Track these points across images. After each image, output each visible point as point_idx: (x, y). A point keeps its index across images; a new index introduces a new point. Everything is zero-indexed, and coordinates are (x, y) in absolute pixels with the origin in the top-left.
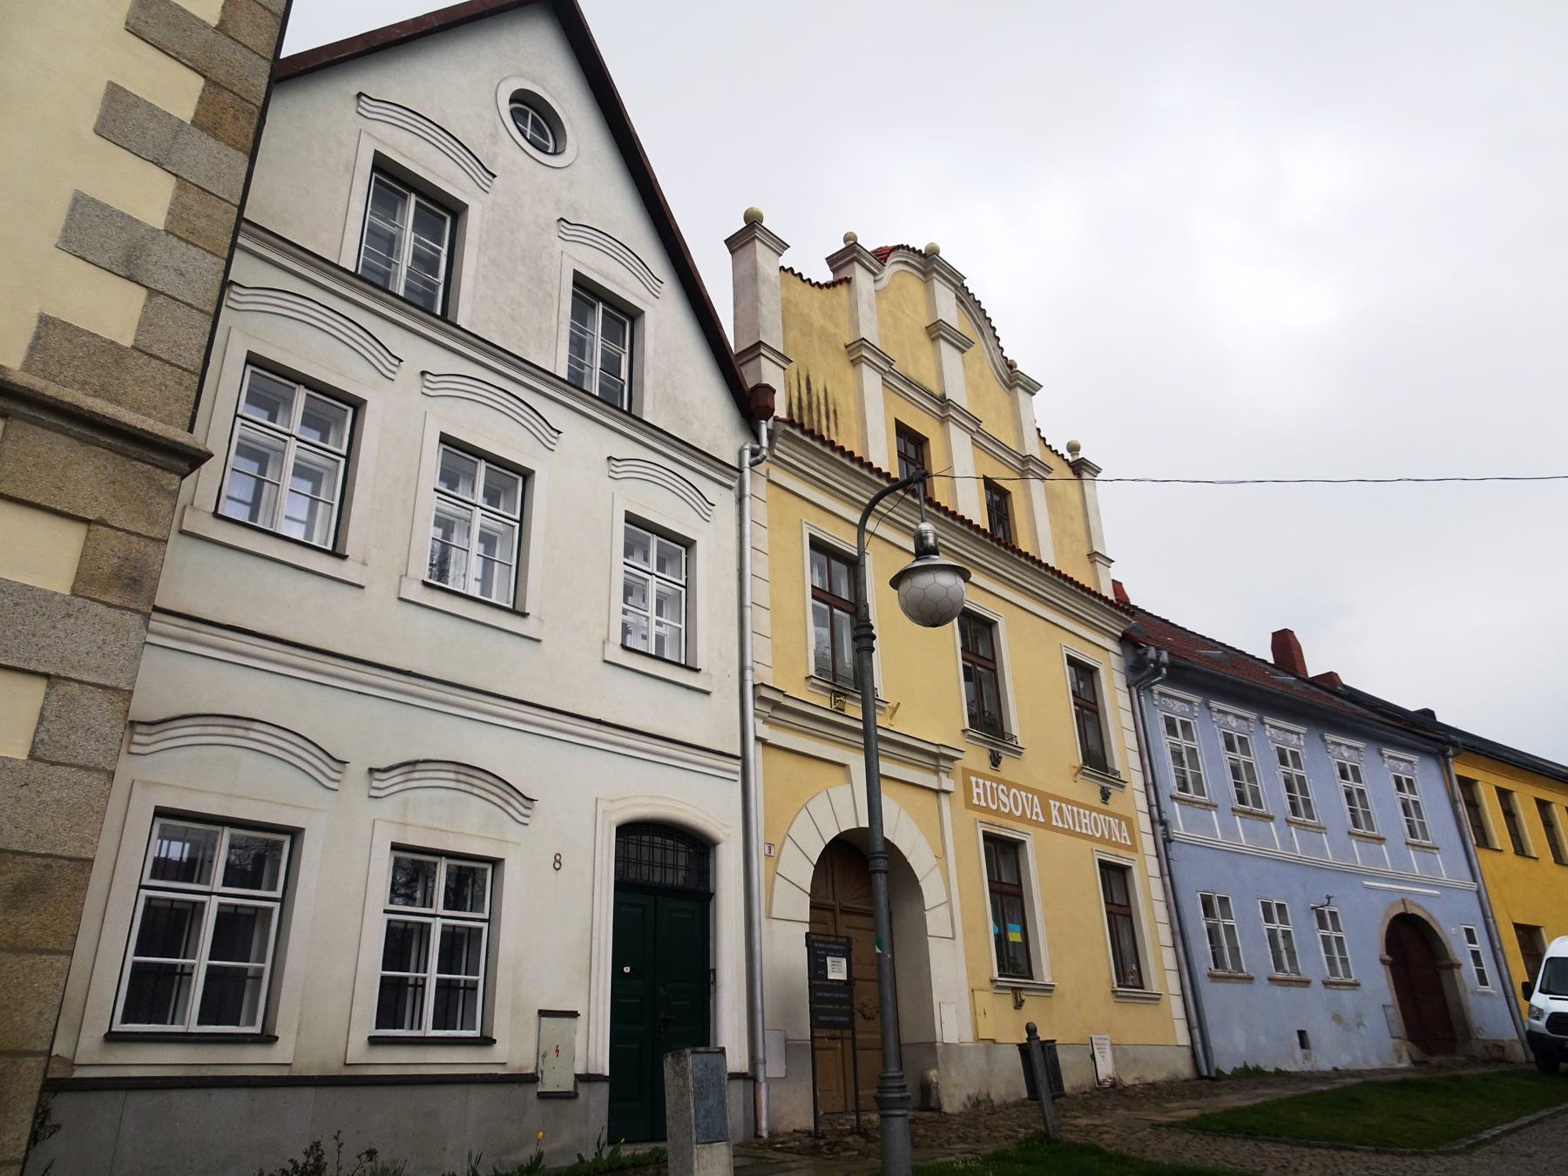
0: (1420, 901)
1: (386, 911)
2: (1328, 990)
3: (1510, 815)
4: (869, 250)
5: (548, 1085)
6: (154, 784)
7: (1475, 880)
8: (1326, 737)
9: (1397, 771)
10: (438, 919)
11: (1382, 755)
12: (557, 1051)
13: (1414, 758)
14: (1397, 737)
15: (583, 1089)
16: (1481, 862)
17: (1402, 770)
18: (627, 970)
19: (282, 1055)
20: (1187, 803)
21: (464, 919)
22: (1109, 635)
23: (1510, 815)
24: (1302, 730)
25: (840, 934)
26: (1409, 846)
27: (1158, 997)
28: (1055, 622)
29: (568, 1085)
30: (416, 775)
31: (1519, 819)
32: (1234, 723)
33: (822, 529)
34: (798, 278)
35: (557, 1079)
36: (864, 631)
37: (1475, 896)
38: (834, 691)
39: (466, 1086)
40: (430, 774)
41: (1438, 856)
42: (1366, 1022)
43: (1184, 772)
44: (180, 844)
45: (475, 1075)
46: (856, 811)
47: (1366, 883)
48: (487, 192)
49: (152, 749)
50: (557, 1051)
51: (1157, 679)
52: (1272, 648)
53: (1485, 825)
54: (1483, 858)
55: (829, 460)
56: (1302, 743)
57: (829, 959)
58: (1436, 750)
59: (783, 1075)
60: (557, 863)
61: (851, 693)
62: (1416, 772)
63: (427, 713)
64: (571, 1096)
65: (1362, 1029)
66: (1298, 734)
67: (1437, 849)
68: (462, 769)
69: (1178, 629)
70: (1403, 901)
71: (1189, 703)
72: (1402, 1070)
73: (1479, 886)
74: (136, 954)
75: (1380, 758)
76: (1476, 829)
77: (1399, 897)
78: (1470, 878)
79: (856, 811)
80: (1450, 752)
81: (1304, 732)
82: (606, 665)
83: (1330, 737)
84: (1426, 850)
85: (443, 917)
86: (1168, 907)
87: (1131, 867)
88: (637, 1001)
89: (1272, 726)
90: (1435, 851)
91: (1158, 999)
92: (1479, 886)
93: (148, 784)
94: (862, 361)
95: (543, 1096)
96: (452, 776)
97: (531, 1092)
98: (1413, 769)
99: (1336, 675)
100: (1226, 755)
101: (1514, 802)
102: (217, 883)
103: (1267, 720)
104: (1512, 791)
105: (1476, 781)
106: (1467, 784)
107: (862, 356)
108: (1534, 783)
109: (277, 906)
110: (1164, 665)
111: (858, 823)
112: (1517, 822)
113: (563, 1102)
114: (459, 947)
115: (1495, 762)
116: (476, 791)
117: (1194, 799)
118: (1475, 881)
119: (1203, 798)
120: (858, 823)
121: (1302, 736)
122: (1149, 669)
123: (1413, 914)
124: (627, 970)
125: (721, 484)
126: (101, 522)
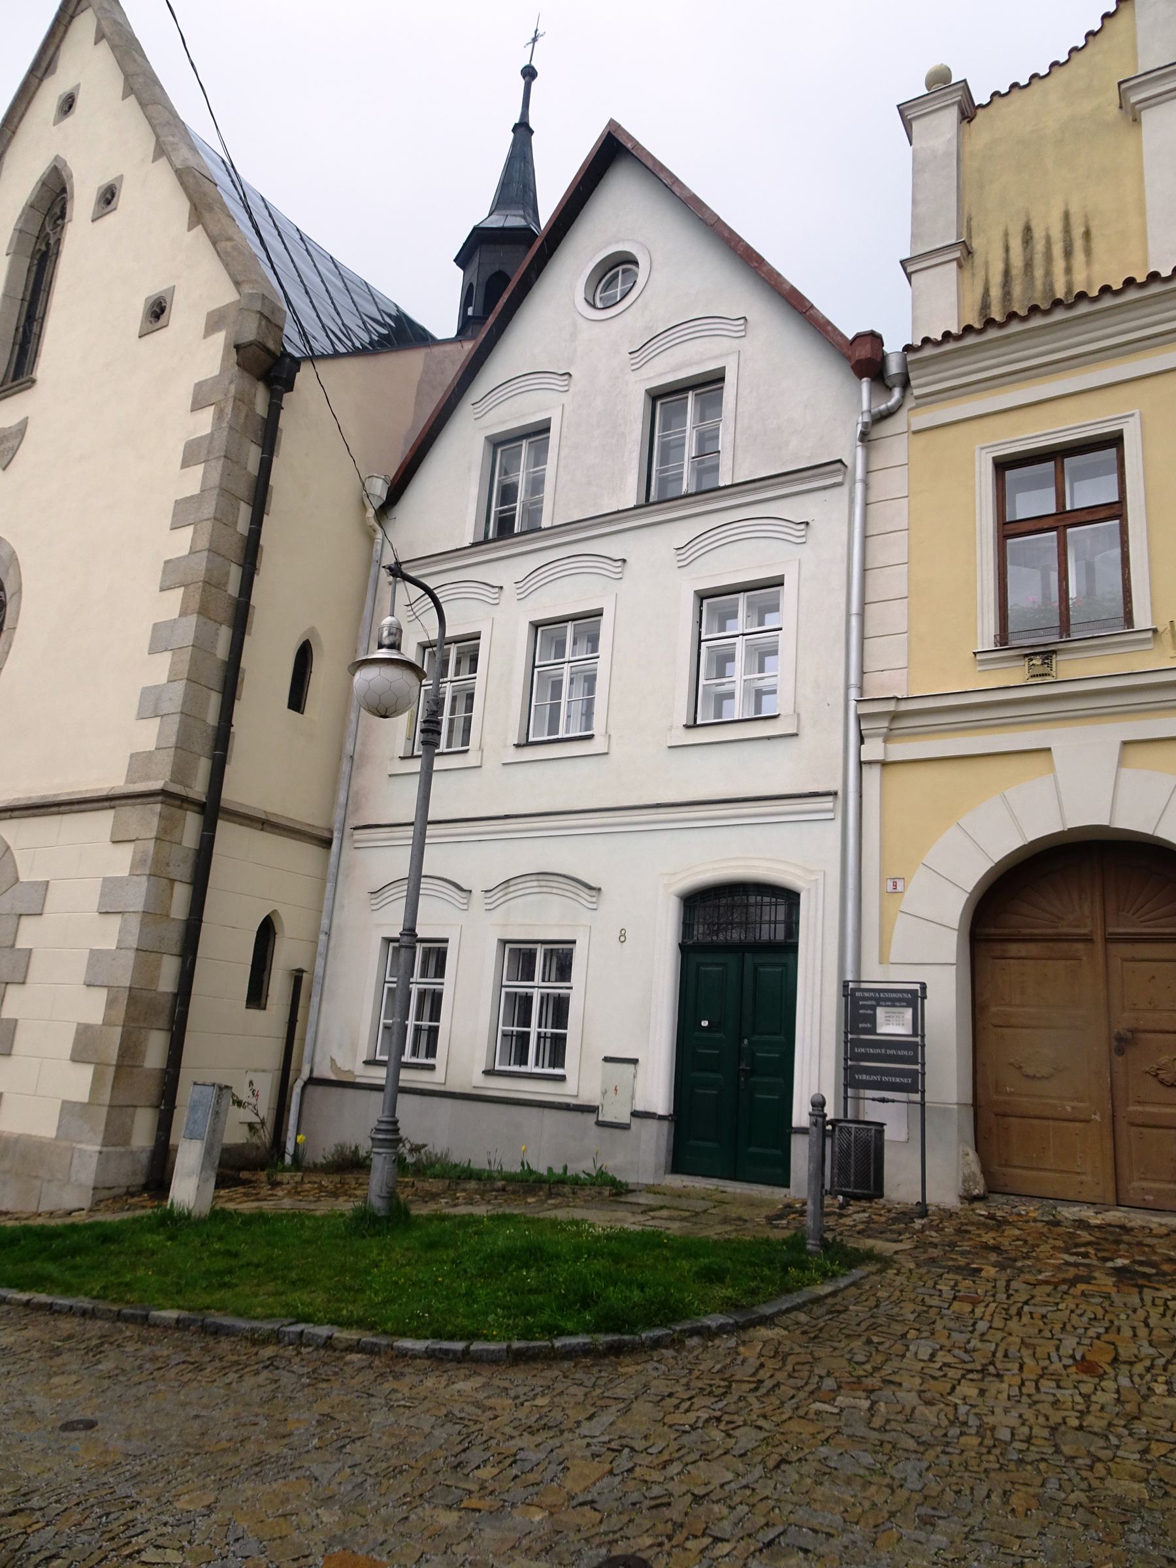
1: (571, 988)
5: (607, 1116)
6: (383, 925)
10: (538, 988)
12: (616, 1090)
15: (636, 1123)
18: (705, 1023)
21: (521, 987)
25: (863, 979)
29: (625, 1118)
30: (511, 889)
33: (1015, 438)
34: (1037, 84)
35: (616, 1112)
36: (430, 737)
38: (1026, 656)
39: (541, 1109)
40: (520, 886)
48: (630, 353)
49: (378, 907)
50: (616, 1090)
55: (1006, 341)
57: (880, 1012)
60: (622, 937)
61: (1061, 646)
63: (516, 842)
64: (625, 1127)
68: (541, 877)
74: (385, 1018)
82: (671, 750)
85: (533, 987)
88: (777, 1055)
93: (378, 925)
95: (600, 1124)
96: (535, 884)
97: (591, 1119)
109: (505, 983)
113: (617, 1132)
114: (559, 1009)
116: (554, 891)
124: (705, 1023)
125: (825, 488)
126: (137, 839)
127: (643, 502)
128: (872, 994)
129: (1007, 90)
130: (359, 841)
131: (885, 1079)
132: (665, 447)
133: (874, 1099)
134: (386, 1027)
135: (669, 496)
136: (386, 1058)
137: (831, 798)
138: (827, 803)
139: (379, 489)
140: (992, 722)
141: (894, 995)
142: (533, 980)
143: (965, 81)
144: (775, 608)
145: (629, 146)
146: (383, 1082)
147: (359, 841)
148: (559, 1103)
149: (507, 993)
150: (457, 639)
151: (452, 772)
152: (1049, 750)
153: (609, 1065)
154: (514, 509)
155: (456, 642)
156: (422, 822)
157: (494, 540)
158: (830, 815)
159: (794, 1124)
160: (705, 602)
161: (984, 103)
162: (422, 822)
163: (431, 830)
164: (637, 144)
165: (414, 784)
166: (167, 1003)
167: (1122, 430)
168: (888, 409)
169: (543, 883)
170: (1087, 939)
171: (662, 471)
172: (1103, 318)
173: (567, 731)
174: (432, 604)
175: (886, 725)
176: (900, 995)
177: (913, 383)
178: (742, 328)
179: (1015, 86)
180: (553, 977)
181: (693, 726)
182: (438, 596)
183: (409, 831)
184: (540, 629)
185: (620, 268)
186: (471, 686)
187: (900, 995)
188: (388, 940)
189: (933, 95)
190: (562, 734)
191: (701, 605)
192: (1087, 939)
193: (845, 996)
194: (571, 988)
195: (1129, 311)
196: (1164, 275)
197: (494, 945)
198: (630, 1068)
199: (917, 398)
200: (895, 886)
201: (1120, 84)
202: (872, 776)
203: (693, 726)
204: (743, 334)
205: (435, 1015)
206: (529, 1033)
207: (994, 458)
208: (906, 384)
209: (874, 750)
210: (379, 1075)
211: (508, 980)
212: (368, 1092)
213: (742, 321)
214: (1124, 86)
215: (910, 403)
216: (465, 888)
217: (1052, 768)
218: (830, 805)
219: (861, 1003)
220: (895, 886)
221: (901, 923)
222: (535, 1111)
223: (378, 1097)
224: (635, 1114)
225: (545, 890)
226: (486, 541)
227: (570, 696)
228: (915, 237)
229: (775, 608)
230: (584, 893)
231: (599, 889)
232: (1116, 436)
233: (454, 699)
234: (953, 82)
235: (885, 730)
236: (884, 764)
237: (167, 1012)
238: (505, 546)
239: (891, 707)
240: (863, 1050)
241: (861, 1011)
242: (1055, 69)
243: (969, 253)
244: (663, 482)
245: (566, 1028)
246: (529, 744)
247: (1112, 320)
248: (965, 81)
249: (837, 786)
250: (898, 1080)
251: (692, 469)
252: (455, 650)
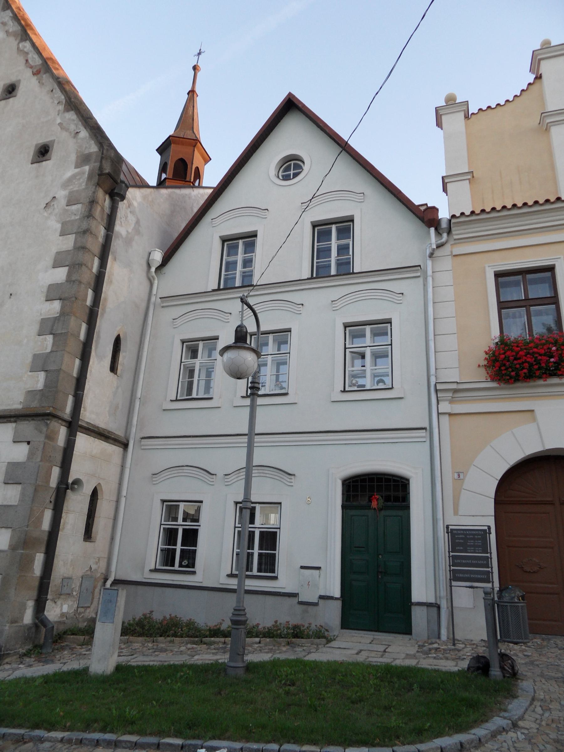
1: (200, 526)
4: (539, 48)
5: (302, 598)
10: (181, 525)
15: (321, 602)
19: (198, 579)
21: (171, 524)
34: (499, 108)
44: (274, 514)
45: (271, 592)
46: (541, 437)
59: (471, 606)
64: (316, 604)
68: (259, 468)
79: (541, 437)
94: (550, 127)
102: (180, 521)
107: (548, 123)
109: (163, 523)
111: (543, 445)
116: (268, 475)
120: (543, 445)
127: (310, 276)
128: (462, 532)
129: (477, 112)
130: (143, 445)
131: (472, 576)
132: (228, 263)
133: (466, 587)
134: (238, 554)
135: (228, 287)
136: (237, 573)
137: (424, 431)
138: (422, 433)
139: (158, 256)
140: (545, 394)
141: (474, 532)
142: (177, 521)
143: (468, 101)
144: (286, 342)
145: (300, 106)
146: (236, 587)
147: (143, 445)
148: (274, 592)
149: (164, 528)
150: (203, 339)
151: (191, 411)
152: (533, 411)
153: (303, 570)
154: (236, 274)
155: (203, 340)
156: (251, 434)
157: (315, 278)
158: (424, 440)
159: (413, 601)
160: (348, 329)
161: (475, 113)
162: (251, 434)
163: (257, 439)
164: (304, 105)
165: (248, 410)
166: (45, 538)
167: (554, 265)
168: (441, 243)
169: (261, 471)
170: (551, 503)
171: (226, 275)
172: (530, 216)
173: (197, 395)
174: (252, 314)
175: (451, 395)
176: (477, 532)
177: (454, 232)
178: (362, 198)
179: (489, 107)
180: (170, 520)
181: (344, 391)
182: (256, 309)
183: (245, 439)
184: (185, 344)
185: (292, 162)
186: (387, 349)
187: (477, 532)
188: (237, 503)
189: (448, 106)
190: (194, 395)
191: (345, 330)
192: (551, 503)
193: (448, 533)
194: (200, 526)
195: (558, 211)
196: (497, 209)
197: (232, 506)
198: (317, 572)
199: (455, 240)
200: (459, 476)
201: (542, 113)
202: (445, 420)
203: (344, 391)
204: (362, 200)
205: (273, 546)
206: (175, 550)
207: (495, 272)
208: (449, 232)
209: (445, 407)
210: (233, 583)
211: (164, 521)
212: (153, 588)
213: (362, 195)
214: (543, 115)
215: (452, 242)
216: (212, 473)
217: (534, 419)
218: (424, 434)
219: (456, 536)
220: (459, 476)
221: (464, 495)
222: (260, 597)
223: (233, 596)
224: (322, 597)
225: (262, 475)
226: (219, 289)
227: (199, 377)
228: (448, 166)
229: (286, 342)
230: (286, 477)
231: (216, 475)
232: (552, 266)
233: (200, 370)
234: (457, 102)
235: (450, 398)
236: (450, 414)
237: (45, 542)
238: (321, 281)
239: (454, 386)
240: (459, 561)
241: (457, 541)
242: (498, 106)
243: (473, 177)
244: (226, 280)
245: (196, 547)
246: (177, 400)
247: (546, 215)
248: (468, 101)
249: (426, 425)
250: (479, 576)
251: (240, 275)
252: (202, 344)
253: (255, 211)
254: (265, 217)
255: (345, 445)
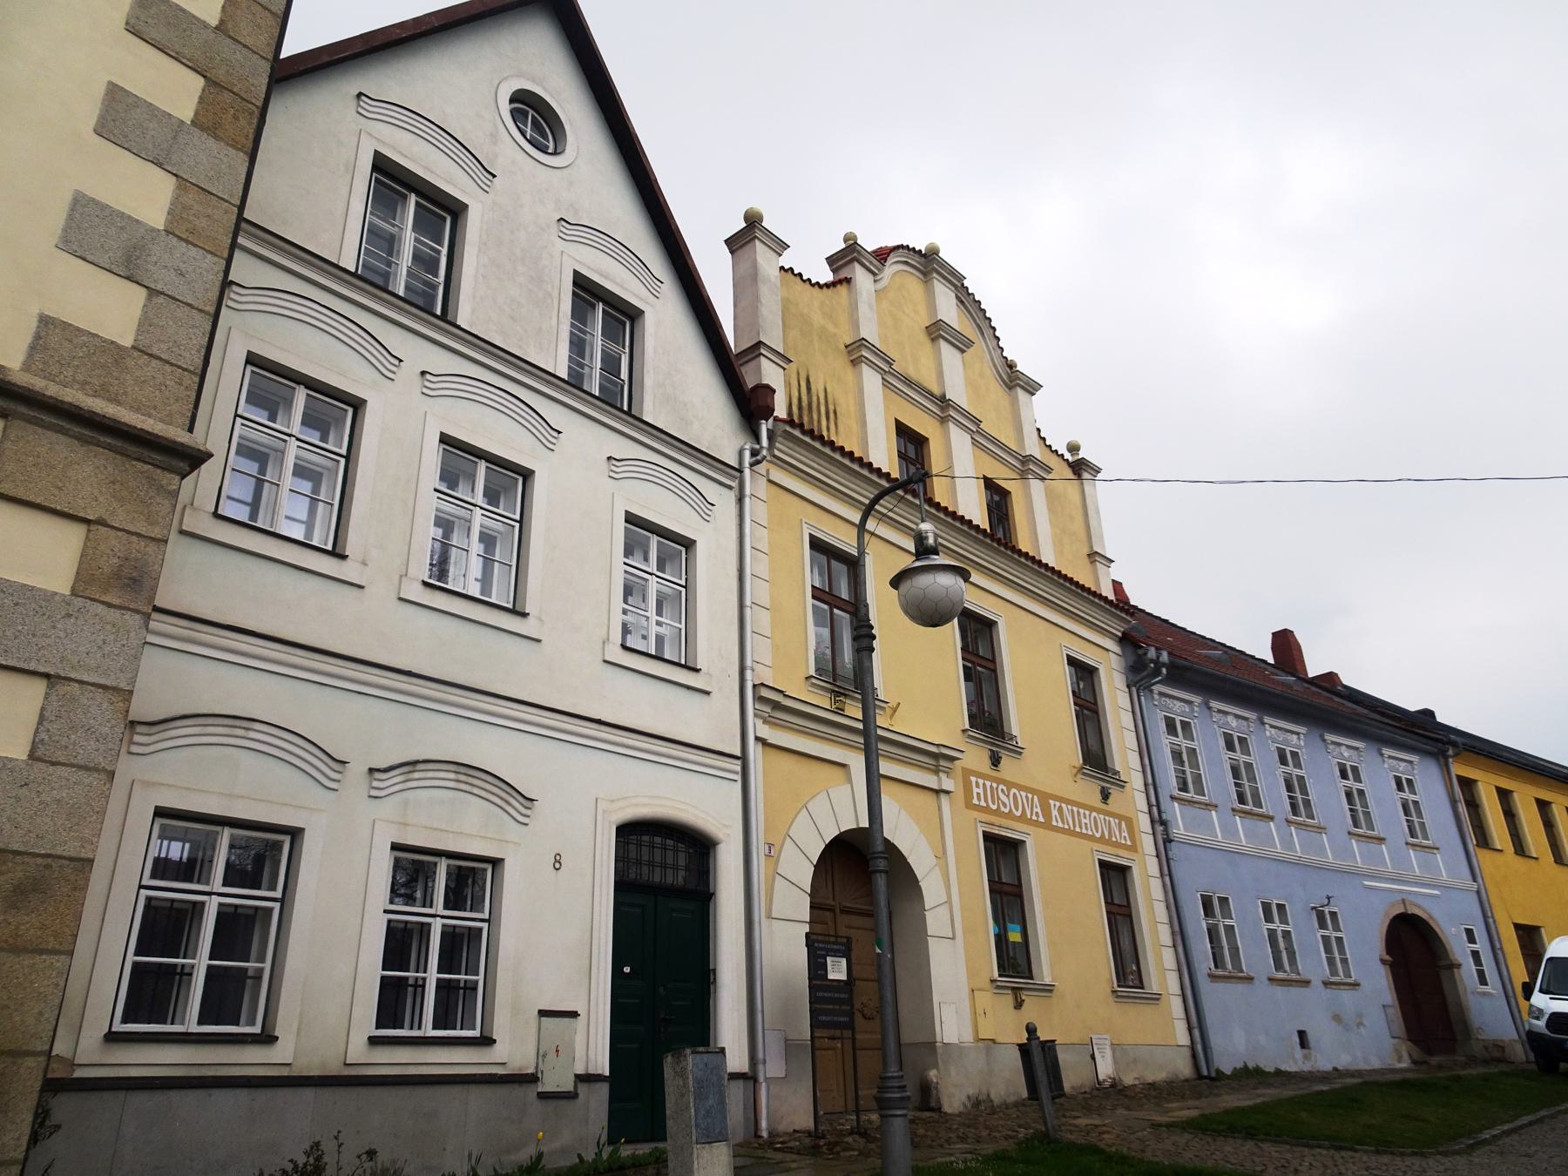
0: (1420, 901)
1: (386, 911)
2: (1328, 990)
3: (1510, 815)
4: (869, 250)
5: (548, 1085)
6: (154, 784)
7: (1475, 880)
8: (1326, 737)
9: (1397, 771)
10: (438, 919)
11: (1382, 755)
12: (557, 1051)
13: (1414, 758)
14: (1397, 737)
15: (583, 1089)
16: (1481, 862)
17: (1402, 770)
18: (627, 970)
19: (282, 1055)
20: (1187, 803)
21: (464, 919)
22: (1109, 635)
23: (1510, 815)
24: (1302, 730)
25: (840, 934)
26: (1409, 846)
27: (1158, 997)
28: (1055, 622)
29: (568, 1085)
30: (416, 775)
31: (1519, 819)
32: (1234, 723)
33: (822, 529)
34: (798, 278)
35: (557, 1079)
36: (864, 631)
37: (1475, 896)
38: (834, 691)
39: (466, 1086)
40: (430, 774)
41: (1438, 856)
42: (1366, 1022)
43: (1184, 772)
44: (180, 844)
45: (475, 1075)
47: (1366, 883)
48: (487, 192)
49: (152, 749)
50: (557, 1051)
51: (1157, 679)
52: (1272, 648)
53: (1485, 825)
54: (1483, 858)
55: (829, 460)
56: (1302, 743)
57: (829, 959)
58: (1436, 750)
59: (783, 1075)
60: (557, 863)
61: (851, 693)
62: (1416, 772)
63: (427, 713)
64: (571, 1096)
65: (1362, 1029)
66: (1298, 734)
67: (1437, 849)
68: (462, 769)
69: (1178, 629)
70: (1403, 901)
71: (1189, 703)
72: (1402, 1070)
73: (1479, 886)
74: (136, 954)
75: (1380, 758)
76: (1476, 829)
77: (1399, 897)
78: (1470, 878)
80: (1450, 752)
81: (1304, 732)
82: (606, 665)
83: (1330, 737)
84: (1426, 850)
85: (443, 917)
86: (1168, 907)
87: (1131, 867)
88: (637, 1001)
89: (1272, 726)
90: (1435, 851)
91: (1158, 999)
92: (1479, 886)
93: (148, 784)
94: (862, 361)
95: (543, 1096)
96: (452, 776)
97: (531, 1092)
98: (1413, 769)
99: (1336, 675)
100: (1226, 755)
101: (1514, 802)
102: (217, 883)
103: (1267, 720)
104: (1512, 791)
105: (1476, 781)
106: (1467, 784)
107: (862, 356)
108: (1534, 783)
109: (277, 906)
110: (1164, 665)
111: (858, 823)
112: (1517, 822)
113: (563, 1102)
114: (459, 947)
115: (1495, 762)
116: (476, 791)
117: (1194, 799)
118: (1475, 881)
119: (1203, 798)
120: (858, 823)
121: (1302, 736)
122: (1149, 669)
123: (1413, 914)
124: (627, 970)
125: (721, 484)
253: (602, 239)
254: (486, 188)
255: (357, 694)
